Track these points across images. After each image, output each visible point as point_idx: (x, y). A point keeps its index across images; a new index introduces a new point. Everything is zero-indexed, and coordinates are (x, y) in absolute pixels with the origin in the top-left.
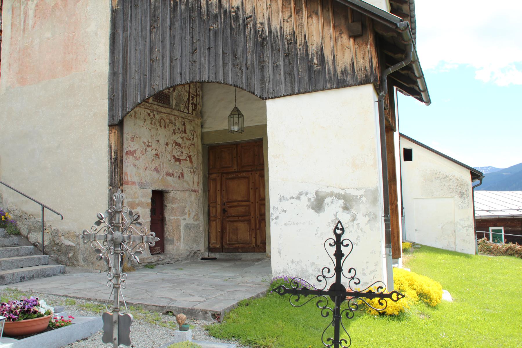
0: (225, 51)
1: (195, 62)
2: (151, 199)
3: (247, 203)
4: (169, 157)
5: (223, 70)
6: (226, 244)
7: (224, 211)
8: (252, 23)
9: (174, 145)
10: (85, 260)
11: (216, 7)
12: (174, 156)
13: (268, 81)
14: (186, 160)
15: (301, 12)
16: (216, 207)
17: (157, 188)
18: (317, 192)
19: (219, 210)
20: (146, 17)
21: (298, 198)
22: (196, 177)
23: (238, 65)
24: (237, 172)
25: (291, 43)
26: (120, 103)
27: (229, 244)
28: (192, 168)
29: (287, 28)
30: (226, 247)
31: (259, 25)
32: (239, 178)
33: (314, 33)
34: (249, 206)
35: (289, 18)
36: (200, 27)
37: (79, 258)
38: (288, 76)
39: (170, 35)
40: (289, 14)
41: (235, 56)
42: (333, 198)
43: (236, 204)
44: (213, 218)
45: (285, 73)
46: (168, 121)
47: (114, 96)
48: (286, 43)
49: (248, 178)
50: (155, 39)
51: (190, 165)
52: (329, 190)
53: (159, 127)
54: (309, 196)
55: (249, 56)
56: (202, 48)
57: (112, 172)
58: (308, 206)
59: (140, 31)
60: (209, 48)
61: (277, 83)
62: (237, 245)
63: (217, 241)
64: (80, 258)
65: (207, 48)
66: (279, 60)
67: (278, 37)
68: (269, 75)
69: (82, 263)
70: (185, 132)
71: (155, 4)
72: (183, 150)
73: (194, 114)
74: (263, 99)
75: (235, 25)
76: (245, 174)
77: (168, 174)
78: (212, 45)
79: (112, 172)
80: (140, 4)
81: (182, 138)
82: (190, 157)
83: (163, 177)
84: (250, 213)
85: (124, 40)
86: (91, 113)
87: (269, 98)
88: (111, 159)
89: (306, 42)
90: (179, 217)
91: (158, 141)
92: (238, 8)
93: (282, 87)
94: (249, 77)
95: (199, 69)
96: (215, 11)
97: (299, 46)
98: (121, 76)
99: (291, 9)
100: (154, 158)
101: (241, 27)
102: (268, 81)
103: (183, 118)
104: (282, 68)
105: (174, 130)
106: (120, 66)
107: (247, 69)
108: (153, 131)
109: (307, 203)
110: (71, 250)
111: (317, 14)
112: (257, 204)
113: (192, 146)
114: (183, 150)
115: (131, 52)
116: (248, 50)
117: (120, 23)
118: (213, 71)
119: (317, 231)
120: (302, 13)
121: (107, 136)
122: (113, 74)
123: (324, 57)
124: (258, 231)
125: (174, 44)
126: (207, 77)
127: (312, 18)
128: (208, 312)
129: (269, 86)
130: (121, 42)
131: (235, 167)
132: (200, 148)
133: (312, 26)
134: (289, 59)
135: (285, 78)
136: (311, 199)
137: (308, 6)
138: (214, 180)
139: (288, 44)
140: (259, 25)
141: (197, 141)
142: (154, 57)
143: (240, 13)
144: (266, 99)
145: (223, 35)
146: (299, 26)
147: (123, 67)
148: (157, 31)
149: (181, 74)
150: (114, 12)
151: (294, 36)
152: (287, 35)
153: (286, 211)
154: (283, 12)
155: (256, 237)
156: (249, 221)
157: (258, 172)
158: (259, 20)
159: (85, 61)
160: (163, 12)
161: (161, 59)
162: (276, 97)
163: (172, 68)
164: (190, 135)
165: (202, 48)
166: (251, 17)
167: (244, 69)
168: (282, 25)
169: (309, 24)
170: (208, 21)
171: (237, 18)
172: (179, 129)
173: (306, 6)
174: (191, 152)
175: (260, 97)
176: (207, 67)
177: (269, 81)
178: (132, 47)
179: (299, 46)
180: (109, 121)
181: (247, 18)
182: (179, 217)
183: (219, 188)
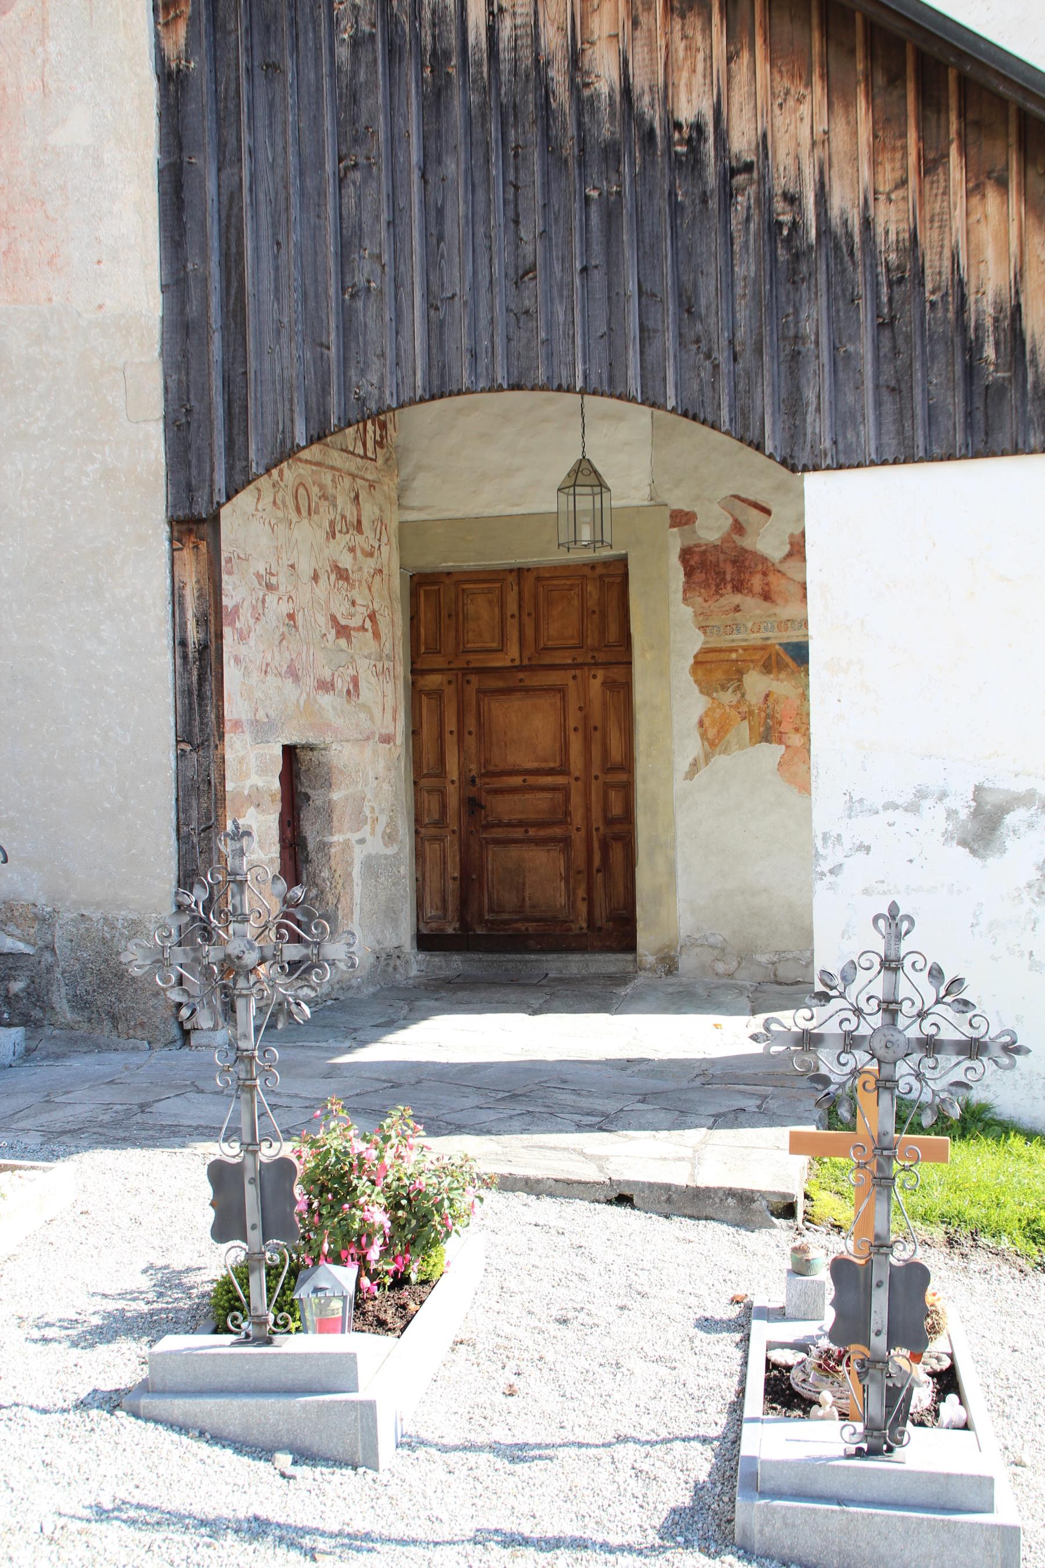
0: (647, 287)
1: (527, 312)
2: (281, 777)
3: (561, 780)
4: (322, 620)
5: (642, 353)
6: (481, 921)
7: (473, 805)
8: (752, 190)
9: (333, 577)
10: (79, 1003)
11: (612, 115)
12: (334, 618)
13: (812, 408)
14: (363, 628)
15: (940, 170)
16: (442, 793)
17: (287, 743)
18: (978, 790)
19: (453, 801)
20: (317, 120)
21: (912, 808)
22: (389, 688)
23: (698, 341)
24: (521, 668)
25: (901, 280)
26: (219, 441)
27: (493, 922)
28: (380, 659)
29: (891, 222)
30: (480, 931)
31: (779, 205)
32: (528, 690)
33: (990, 253)
34: (565, 790)
35: (897, 187)
36: (546, 185)
37: (55, 998)
38: (886, 397)
39: (425, 204)
40: (898, 174)
41: (688, 307)
42: (1033, 811)
43: (517, 781)
44: (432, 831)
45: (877, 387)
46: (315, 490)
47: (188, 412)
48: (883, 279)
49: (561, 690)
50: (358, 204)
51: (373, 644)
52: (1020, 786)
53: (293, 515)
54: (951, 802)
55: (743, 313)
56: (557, 268)
57: (190, 693)
58: (947, 836)
59: (292, 171)
60: (584, 270)
61: (844, 420)
62: (521, 926)
63: (445, 908)
64: (59, 998)
65: (578, 266)
66: (855, 338)
67: (851, 254)
68: (816, 389)
69: (65, 1012)
70: (359, 527)
71: (355, 73)
72: (355, 594)
73: (380, 461)
74: (793, 469)
75: (686, 194)
76: (553, 678)
77: (325, 686)
78: (597, 258)
79: (190, 693)
80: (289, 64)
81: (352, 550)
82: (372, 617)
83: (308, 694)
84: (567, 813)
85: (225, 199)
86: (90, 468)
87: (816, 468)
88: (183, 643)
89: (961, 281)
90: (348, 835)
91: (292, 566)
92: (698, 128)
93: (869, 429)
94: (741, 386)
95: (547, 342)
96: (606, 129)
97: (933, 292)
98: (217, 338)
99: (905, 155)
100: (285, 629)
101: (713, 204)
102: (812, 408)
103: (354, 476)
104: (868, 370)
105: (332, 524)
106: (215, 301)
107: (735, 359)
108: (281, 529)
109: (942, 824)
110: (15, 969)
111: (1002, 184)
112: (594, 785)
113: (378, 578)
114: (355, 594)
115: (257, 249)
116: (739, 291)
117: (203, 127)
118: (599, 352)
119: (975, 915)
120: (947, 173)
121: (165, 560)
122: (182, 331)
123: (1023, 342)
124: (599, 878)
125: (440, 238)
126: (579, 373)
127: (984, 196)
128: (757, 1196)
129: (818, 426)
130: (212, 207)
131: (513, 651)
132: (396, 582)
133: (982, 227)
134: (894, 339)
135: (878, 404)
136: (956, 812)
137: (972, 151)
138: (437, 694)
139: (890, 284)
140: (779, 205)
141: (389, 557)
142: (360, 279)
143: (709, 147)
144: (805, 469)
145: (639, 223)
146: (932, 221)
147: (224, 304)
148: (365, 181)
149: (474, 355)
150: (171, 81)
151: (916, 259)
152: (887, 251)
153: (868, 849)
154: (875, 164)
155: (590, 900)
156: (566, 842)
157: (600, 673)
158: (780, 183)
159: (50, 263)
160: (392, 109)
161: (389, 289)
162: (840, 467)
163: (436, 331)
164: (371, 535)
165: (557, 268)
166: (748, 167)
167: (722, 357)
168: (872, 212)
169: (973, 218)
170: (582, 164)
171: (694, 161)
172: (343, 517)
173: (963, 150)
174: (376, 600)
175: (783, 463)
176: (579, 341)
177: (818, 410)
178: (263, 233)
179: (933, 292)
180: (173, 505)
181: (734, 172)
182: (348, 835)
183: (451, 724)
